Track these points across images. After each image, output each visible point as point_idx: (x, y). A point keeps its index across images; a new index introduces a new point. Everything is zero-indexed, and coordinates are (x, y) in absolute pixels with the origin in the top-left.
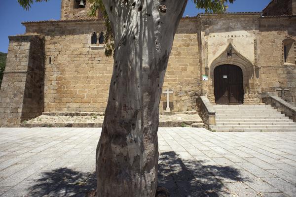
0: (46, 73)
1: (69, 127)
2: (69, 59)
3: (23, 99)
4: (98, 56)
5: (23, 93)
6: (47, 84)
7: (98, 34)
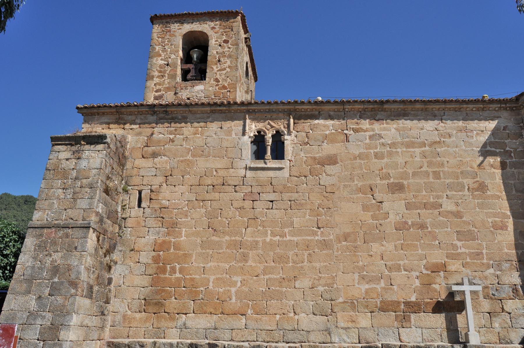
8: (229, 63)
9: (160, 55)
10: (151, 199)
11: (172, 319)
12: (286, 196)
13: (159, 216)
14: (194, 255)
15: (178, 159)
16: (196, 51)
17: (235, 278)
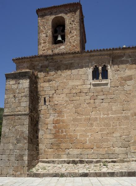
0: (41, 116)
1: (84, 176)
2: (67, 99)
3: (27, 145)
4: (101, 93)
5: (27, 137)
6: (43, 128)
7: (100, 68)
8: (75, 33)
9: (43, 31)
10: (50, 101)
11: (64, 151)
12: (109, 97)
13: (54, 108)
14: (70, 125)
15: (60, 81)
16: (59, 29)
17: (88, 134)
